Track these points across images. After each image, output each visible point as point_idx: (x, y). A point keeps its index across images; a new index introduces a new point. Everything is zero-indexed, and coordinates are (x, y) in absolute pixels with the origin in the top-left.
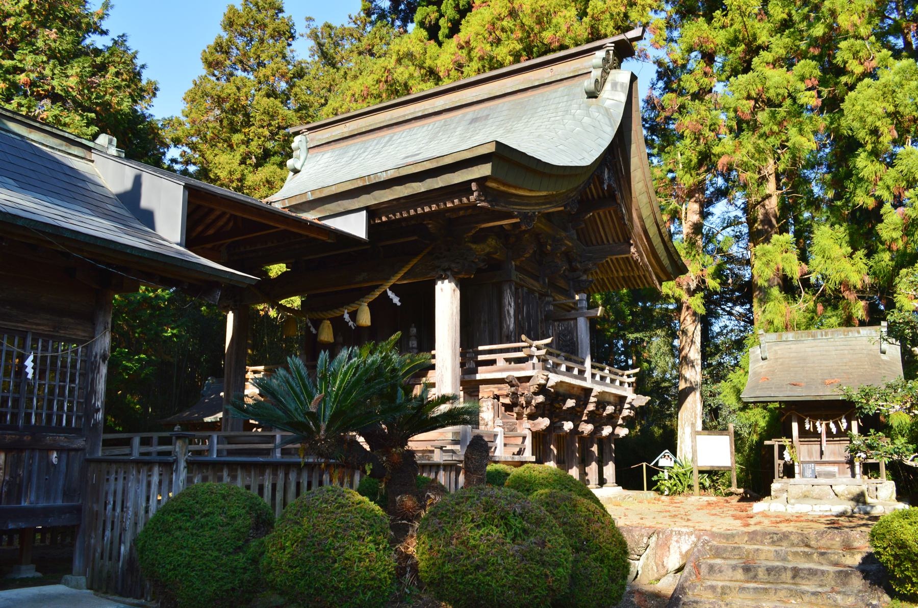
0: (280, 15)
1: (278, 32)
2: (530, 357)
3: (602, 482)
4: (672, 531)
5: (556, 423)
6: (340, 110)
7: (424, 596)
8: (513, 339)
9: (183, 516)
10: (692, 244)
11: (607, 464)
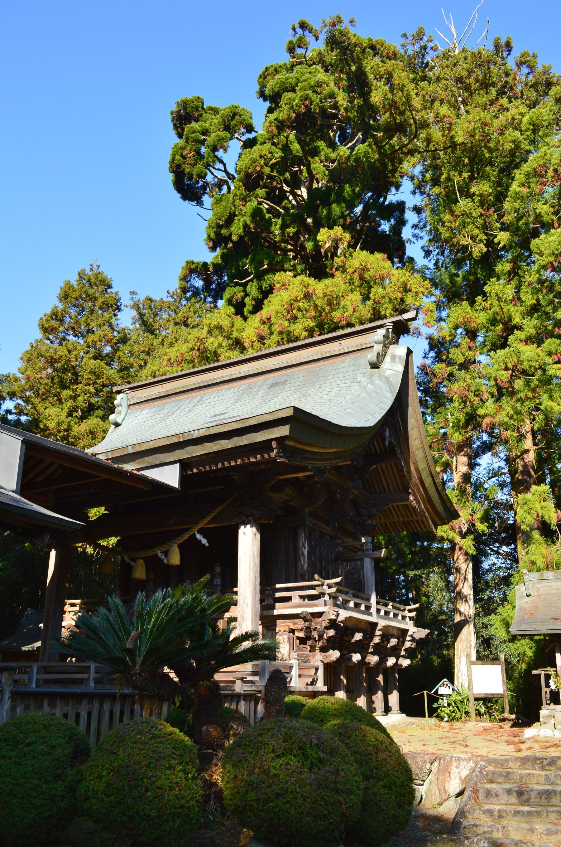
0: (109, 290)
1: (107, 305)
2: (322, 595)
3: (387, 710)
4: (452, 757)
5: (345, 654)
6: (157, 373)
7: (227, 823)
8: (307, 577)
9: (8, 745)
10: (463, 492)
11: (391, 693)
